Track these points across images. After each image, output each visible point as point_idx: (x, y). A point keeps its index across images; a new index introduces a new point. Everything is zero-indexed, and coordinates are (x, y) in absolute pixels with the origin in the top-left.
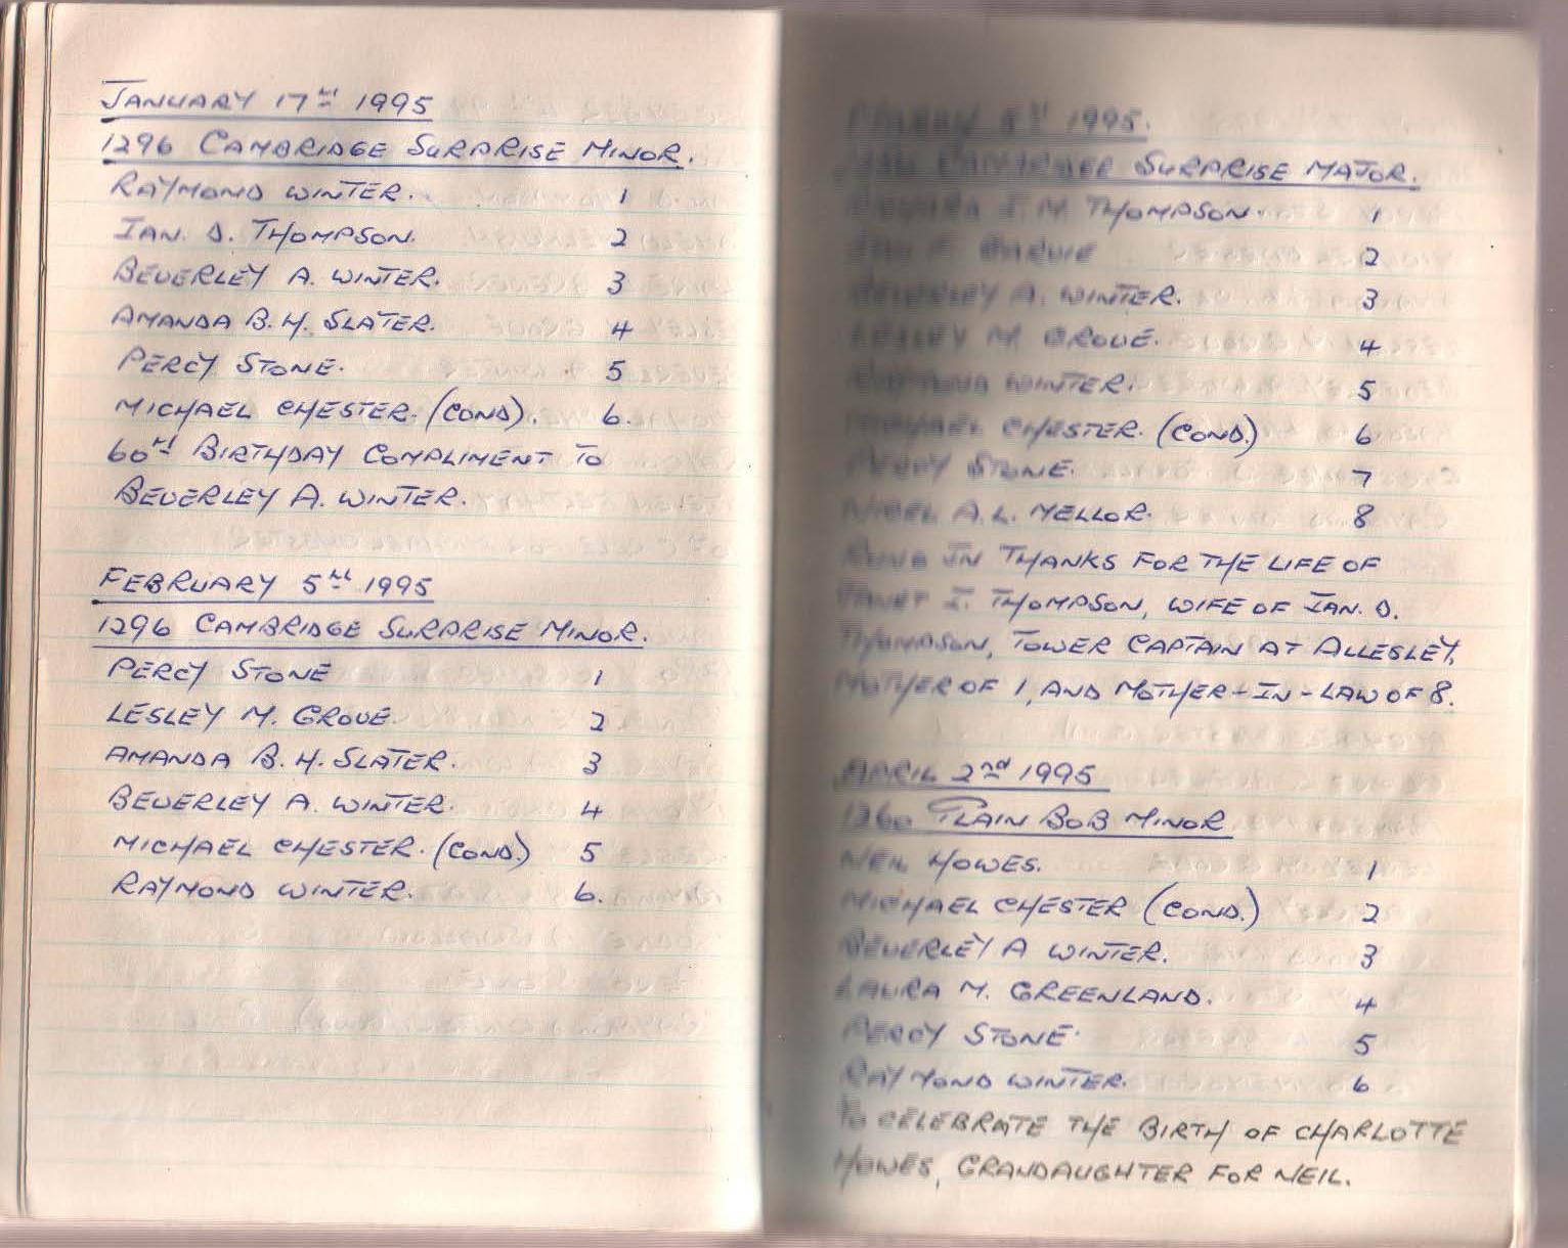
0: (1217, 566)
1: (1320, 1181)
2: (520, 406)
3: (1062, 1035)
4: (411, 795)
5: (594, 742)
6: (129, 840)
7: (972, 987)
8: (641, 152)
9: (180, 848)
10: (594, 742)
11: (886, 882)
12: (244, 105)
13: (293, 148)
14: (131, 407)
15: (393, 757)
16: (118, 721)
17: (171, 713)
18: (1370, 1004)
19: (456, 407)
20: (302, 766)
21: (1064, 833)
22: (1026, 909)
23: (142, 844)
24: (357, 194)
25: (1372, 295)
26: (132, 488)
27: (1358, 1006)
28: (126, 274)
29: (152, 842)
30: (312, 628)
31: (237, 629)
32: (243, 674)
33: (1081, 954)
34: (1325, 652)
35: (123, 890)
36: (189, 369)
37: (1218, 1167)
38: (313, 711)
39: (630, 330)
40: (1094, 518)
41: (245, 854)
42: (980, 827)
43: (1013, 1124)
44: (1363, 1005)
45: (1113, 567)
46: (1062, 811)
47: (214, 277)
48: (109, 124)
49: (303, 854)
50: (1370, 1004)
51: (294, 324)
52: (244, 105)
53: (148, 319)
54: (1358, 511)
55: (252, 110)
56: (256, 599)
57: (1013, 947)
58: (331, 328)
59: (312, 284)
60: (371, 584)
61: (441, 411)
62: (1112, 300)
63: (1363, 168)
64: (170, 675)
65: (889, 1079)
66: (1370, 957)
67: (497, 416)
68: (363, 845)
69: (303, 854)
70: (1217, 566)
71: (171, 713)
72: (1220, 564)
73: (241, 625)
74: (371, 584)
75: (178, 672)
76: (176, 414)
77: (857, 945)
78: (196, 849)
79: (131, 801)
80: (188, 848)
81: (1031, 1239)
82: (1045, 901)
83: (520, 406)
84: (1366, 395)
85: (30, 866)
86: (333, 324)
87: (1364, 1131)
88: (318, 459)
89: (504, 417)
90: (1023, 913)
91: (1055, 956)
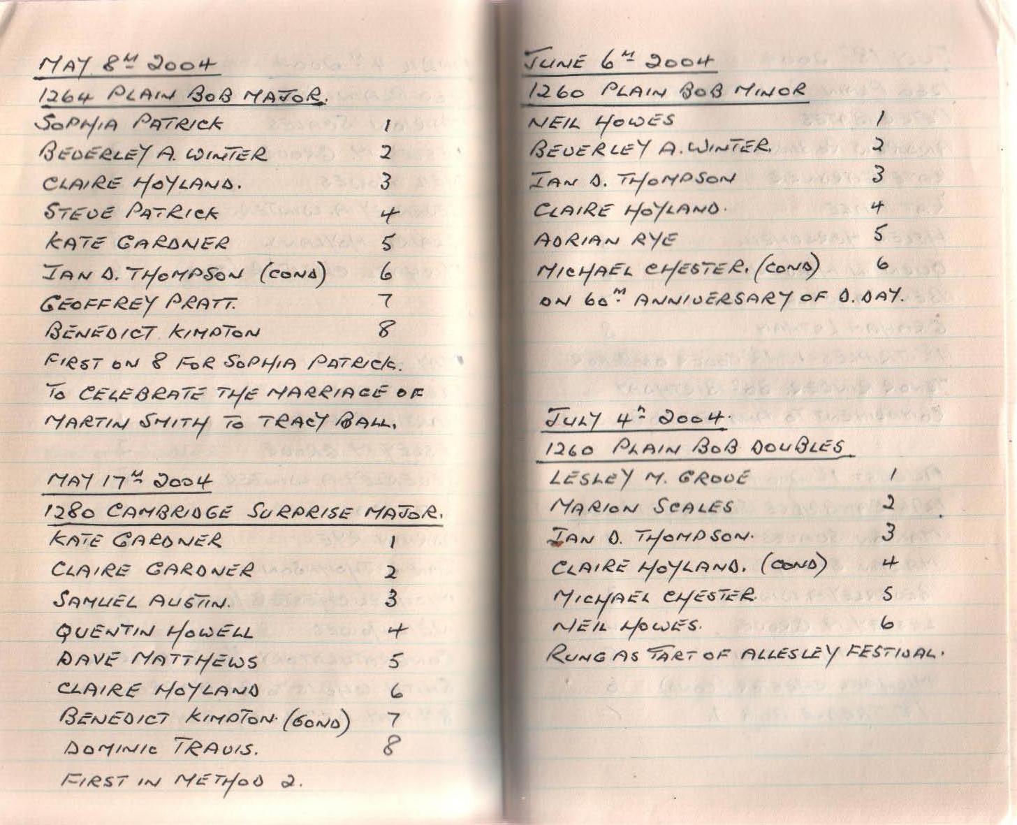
4: (161, 723)
5: (385, 166)
6: (566, 502)
8: (610, 507)
9: (267, 364)
10: (385, 166)
11: (564, 137)
14: (187, 780)
15: (732, 144)
18: (880, 205)
19: (278, 271)
20: (645, 573)
21: (166, 491)
22: (602, 122)
23: (117, 749)
26: (687, 89)
27: (873, 207)
28: (49, 155)
29: (803, 263)
33: (647, 94)
36: (83, 396)
38: (158, 566)
39: (630, 421)
41: (931, 656)
44: (876, 206)
47: (113, 155)
49: (236, 398)
50: (880, 205)
54: (156, 356)
56: (590, 430)
57: (665, 148)
58: (145, 427)
60: (125, 333)
61: (268, 272)
62: (727, 148)
63: (403, 510)
64: (111, 157)
66: (891, 532)
68: (184, 422)
69: (236, 398)
74: (125, 333)
75: (133, 332)
78: (62, 419)
79: (62, 332)
80: (590, 272)
81: (16, 13)
86: (147, 424)
88: (161, 604)
90: (681, 602)
91: (693, 150)
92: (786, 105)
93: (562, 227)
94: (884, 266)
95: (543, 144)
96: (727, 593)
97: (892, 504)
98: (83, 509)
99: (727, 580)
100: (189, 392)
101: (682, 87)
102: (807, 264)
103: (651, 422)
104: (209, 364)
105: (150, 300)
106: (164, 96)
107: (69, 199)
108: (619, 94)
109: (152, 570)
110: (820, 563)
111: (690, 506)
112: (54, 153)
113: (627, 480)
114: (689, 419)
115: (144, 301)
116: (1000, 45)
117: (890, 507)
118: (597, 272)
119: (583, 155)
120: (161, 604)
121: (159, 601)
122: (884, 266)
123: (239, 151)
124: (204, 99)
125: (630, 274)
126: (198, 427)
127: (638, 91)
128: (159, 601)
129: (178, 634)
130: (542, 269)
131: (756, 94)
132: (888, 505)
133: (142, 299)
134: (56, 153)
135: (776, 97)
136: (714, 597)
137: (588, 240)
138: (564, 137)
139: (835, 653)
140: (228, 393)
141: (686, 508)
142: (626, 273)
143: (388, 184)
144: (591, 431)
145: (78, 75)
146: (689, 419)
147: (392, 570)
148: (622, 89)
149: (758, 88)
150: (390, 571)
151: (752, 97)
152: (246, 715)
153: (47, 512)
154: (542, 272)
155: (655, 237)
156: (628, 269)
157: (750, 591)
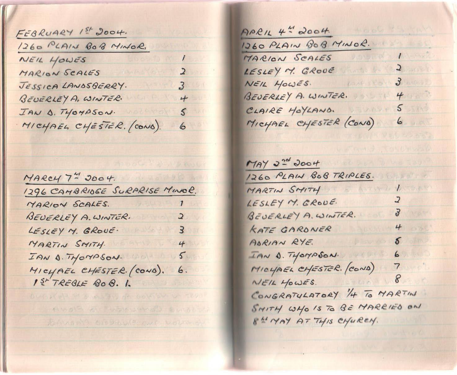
0: (314, 191)
1: (302, 295)
2: (373, 265)
3: (273, 230)
7: (299, 189)
9: (306, 124)
11: (259, 91)
12: (70, 34)
13: (37, 34)
16: (66, 88)
17: (49, 231)
24: (327, 270)
25: (399, 80)
28: (24, 101)
30: (91, 191)
31: (66, 193)
32: (83, 271)
33: (327, 217)
34: (340, 173)
35: (33, 270)
37: (20, 31)
40: (284, 217)
42: (285, 49)
43: (264, 230)
45: (330, 59)
46: (312, 42)
48: (20, 59)
51: (301, 309)
52: (70, 34)
53: (89, 256)
55: (73, 35)
59: (160, 129)
65: (286, 322)
66: (399, 212)
67: (151, 128)
70: (314, 191)
71: (49, 231)
72: (314, 190)
73: (67, 191)
76: (43, 127)
77: (250, 97)
82: (97, 269)
83: (373, 265)
84: (120, 192)
85: (4, 312)
87: (360, 321)
88: (86, 219)
89: (155, 271)
92: (357, 51)
93: (258, 105)
94: (400, 123)
95: (249, 94)
96: (327, 122)
97: (399, 201)
98: (48, 177)
99: (326, 116)
100: (329, 308)
101: (311, 174)
102: (369, 267)
103: (295, 33)
104: (62, 283)
105: (75, 216)
106: (73, 47)
107: (33, 80)
108: (283, 178)
109: (305, 204)
110: (372, 268)
111: (311, 57)
112: (26, 99)
113: (75, 218)
114: (313, 32)
115: (71, 216)
116: (454, 24)
117: (399, 70)
118: (273, 124)
119: (266, 99)
120: (86, 219)
121: (85, 218)
122: (400, 123)
123: (110, 124)
124: (92, 48)
125: (288, 126)
126: (295, 258)
127: (291, 176)
128: (85, 218)
129: (286, 283)
130: (249, 122)
131: (343, 45)
132: (397, 201)
133: (71, 215)
134: (27, 100)
135: (352, 47)
136: (321, 124)
137: (271, 243)
138: (259, 91)
139: (23, 109)
140: (97, 244)
141: (310, 58)
142: (286, 126)
143: (183, 86)
144: (36, 197)
145: (36, 196)
146: (313, 32)
147: (183, 70)
148: (284, 176)
149: (344, 43)
150: (182, 71)
151: (341, 47)
152: (339, 215)
153: (35, 284)
154: (249, 123)
155: (302, 240)
156: (286, 124)
157: (338, 266)
